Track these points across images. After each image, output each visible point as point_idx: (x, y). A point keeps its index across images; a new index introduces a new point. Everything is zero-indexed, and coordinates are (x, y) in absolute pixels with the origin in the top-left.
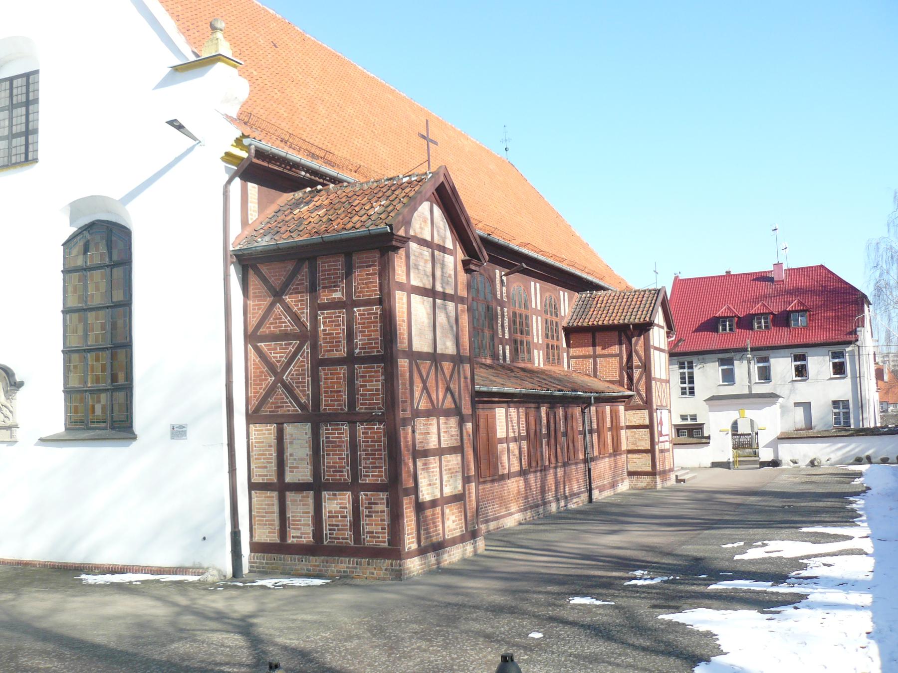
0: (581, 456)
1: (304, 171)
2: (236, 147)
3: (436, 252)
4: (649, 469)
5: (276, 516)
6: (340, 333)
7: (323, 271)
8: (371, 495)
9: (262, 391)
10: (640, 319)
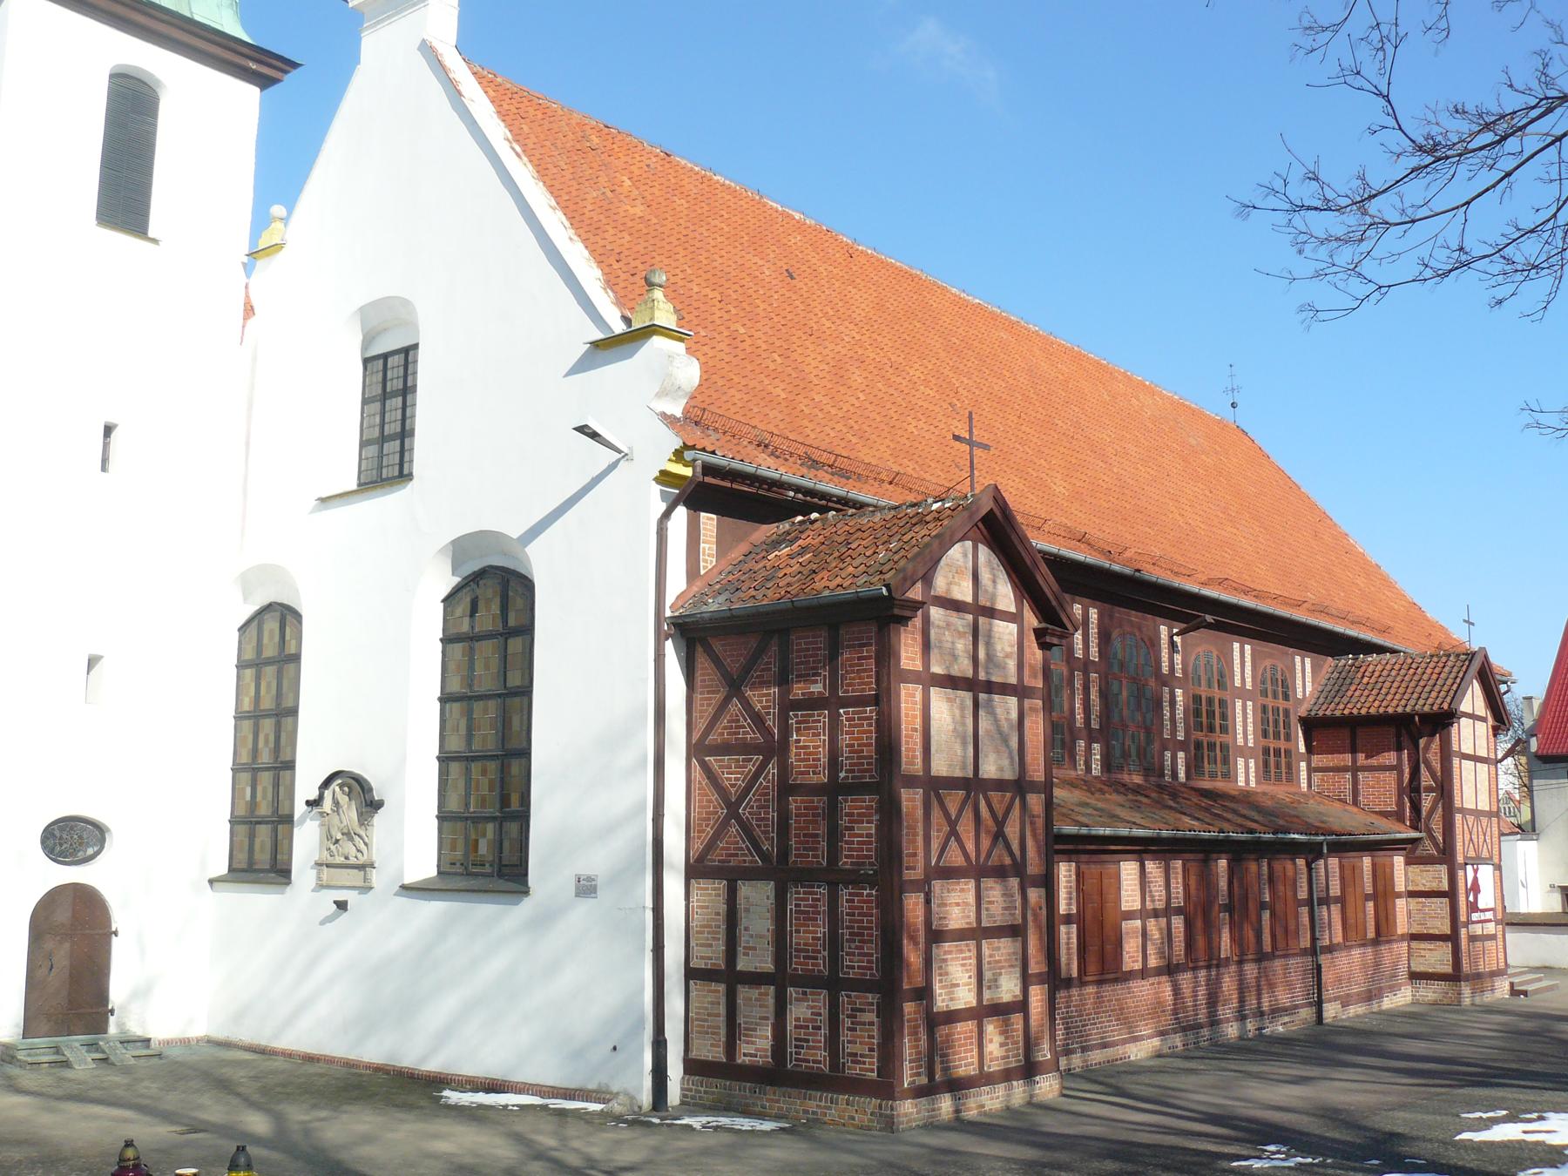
0: (1305, 942)
1: (792, 490)
2: (676, 462)
3: (981, 620)
4: (1448, 969)
5: (721, 1021)
6: (819, 746)
7: (798, 651)
8: (856, 997)
9: (709, 829)
10: (1433, 705)
